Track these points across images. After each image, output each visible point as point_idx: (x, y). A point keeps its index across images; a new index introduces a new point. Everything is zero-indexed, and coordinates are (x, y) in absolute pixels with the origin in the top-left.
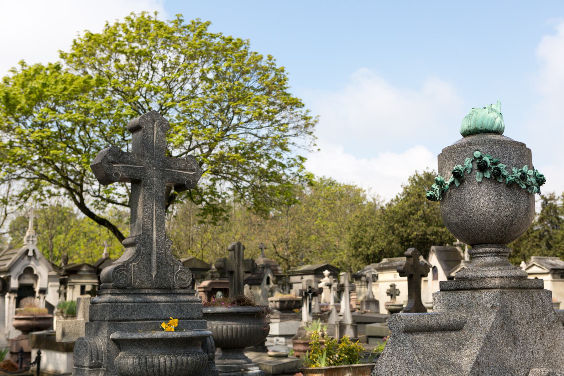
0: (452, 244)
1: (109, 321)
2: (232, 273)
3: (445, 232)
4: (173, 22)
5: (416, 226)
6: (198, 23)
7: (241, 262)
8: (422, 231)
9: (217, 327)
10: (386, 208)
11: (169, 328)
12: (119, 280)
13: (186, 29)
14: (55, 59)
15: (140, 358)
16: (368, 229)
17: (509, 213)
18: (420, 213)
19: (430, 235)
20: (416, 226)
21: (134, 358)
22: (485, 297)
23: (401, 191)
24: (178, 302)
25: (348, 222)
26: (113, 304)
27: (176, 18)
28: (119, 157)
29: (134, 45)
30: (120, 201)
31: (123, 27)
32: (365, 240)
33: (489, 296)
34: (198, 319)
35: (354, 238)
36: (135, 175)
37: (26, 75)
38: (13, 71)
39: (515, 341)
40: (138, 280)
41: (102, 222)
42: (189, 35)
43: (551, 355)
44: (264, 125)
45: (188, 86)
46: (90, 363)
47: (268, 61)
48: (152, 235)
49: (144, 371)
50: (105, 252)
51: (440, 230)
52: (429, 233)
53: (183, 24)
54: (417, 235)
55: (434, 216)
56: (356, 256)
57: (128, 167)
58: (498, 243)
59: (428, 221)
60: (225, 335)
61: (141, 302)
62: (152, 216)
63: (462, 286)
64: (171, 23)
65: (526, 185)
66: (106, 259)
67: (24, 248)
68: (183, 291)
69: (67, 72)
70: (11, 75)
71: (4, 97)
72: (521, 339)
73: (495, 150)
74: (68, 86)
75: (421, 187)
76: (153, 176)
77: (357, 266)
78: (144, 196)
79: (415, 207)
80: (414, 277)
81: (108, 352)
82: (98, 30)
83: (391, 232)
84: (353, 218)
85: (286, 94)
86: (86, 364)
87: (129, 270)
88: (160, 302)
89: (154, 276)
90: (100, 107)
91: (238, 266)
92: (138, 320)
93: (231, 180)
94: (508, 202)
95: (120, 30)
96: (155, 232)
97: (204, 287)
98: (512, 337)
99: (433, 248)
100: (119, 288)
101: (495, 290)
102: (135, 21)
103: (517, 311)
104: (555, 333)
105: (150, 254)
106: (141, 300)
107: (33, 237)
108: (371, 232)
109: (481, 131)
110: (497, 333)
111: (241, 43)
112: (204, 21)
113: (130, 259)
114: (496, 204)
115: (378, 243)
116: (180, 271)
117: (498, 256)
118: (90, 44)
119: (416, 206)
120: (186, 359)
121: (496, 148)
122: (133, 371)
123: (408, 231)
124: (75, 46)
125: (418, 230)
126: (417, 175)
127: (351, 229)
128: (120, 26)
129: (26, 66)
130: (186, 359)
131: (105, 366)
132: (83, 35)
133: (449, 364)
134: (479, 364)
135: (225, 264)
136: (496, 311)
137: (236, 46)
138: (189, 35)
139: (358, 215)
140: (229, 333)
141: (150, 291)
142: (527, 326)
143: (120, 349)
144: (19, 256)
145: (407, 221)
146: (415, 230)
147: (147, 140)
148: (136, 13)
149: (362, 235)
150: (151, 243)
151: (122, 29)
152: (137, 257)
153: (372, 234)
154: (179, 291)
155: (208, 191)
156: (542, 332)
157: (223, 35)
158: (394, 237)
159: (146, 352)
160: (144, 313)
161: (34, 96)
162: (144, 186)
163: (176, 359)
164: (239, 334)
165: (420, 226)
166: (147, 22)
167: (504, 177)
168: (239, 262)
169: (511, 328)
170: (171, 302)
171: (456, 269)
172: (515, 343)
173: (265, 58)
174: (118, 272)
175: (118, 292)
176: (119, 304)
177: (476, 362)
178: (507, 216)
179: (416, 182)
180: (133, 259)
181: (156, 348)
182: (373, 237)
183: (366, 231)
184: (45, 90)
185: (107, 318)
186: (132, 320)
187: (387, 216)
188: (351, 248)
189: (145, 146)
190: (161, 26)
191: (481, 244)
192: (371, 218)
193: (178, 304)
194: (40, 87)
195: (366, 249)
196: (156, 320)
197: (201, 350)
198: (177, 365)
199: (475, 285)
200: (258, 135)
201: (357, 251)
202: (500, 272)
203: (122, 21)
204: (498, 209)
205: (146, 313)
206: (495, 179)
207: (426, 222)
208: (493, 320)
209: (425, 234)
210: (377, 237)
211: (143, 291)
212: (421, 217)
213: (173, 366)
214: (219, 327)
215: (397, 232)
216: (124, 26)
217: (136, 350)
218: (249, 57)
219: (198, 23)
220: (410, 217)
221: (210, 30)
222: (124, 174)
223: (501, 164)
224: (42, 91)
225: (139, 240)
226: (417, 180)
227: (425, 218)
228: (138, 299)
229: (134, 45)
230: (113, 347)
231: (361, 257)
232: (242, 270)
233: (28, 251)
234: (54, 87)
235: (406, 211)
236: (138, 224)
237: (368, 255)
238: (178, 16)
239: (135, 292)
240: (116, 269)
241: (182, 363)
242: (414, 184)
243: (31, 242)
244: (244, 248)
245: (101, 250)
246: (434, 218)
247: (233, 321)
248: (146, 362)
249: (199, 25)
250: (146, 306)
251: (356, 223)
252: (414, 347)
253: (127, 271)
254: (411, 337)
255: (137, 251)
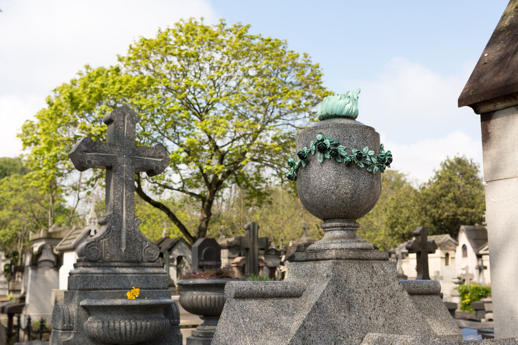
0: (481, 224)
1: (80, 290)
2: (247, 249)
3: (475, 212)
4: (217, 26)
5: (447, 208)
6: (239, 27)
7: (256, 240)
8: (453, 211)
9: (197, 297)
10: (419, 191)
11: (132, 297)
12: (90, 254)
13: (229, 32)
14: (115, 63)
15: (104, 322)
16: (403, 210)
17: (348, 191)
18: (451, 195)
19: (460, 215)
20: (447, 208)
21: (98, 322)
22: (324, 267)
23: (433, 175)
24: (145, 274)
25: (385, 204)
26: (84, 275)
27: (219, 23)
28: (92, 147)
29: (183, 48)
30: (175, 187)
31: (174, 32)
32: (400, 220)
33: (326, 266)
34: (163, 288)
35: (390, 218)
36: (107, 162)
37: (89, 77)
38: (80, 74)
39: (350, 307)
40: (108, 254)
41: (157, 205)
42: (232, 38)
43: (392, 322)
44: (299, 117)
45: (233, 83)
46: (62, 326)
47: (304, 59)
48: (122, 214)
49: (107, 334)
50: (164, 231)
51: (470, 210)
52: (459, 213)
53: (226, 28)
54: (448, 216)
55: (464, 197)
56: (392, 235)
57: (100, 155)
58: (344, 218)
59: (459, 203)
60: (204, 304)
61: (110, 273)
62: (123, 198)
63: (310, 257)
64: (215, 27)
65: (364, 164)
66: (166, 238)
67: (86, 229)
68: (150, 264)
69: (126, 74)
70: (78, 77)
71: (68, 96)
72: (357, 307)
73: (336, 133)
74: (123, 87)
75: (451, 171)
76: (124, 164)
77: (394, 245)
78: (115, 180)
79: (446, 190)
80: (422, 254)
81: (78, 316)
82: (152, 35)
83: (423, 213)
84: (389, 200)
85: (321, 88)
86: (60, 327)
87: (101, 245)
88: (128, 274)
89: (123, 251)
90: (151, 104)
91: (253, 243)
92: (106, 289)
93: (272, 167)
94: (346, 181)
95: (170, 35)
96: (124, 212)
97: (237, 263)
98: (346, 305)
99: (463, 227)
100: (90, 261)
101: (330, 261)
102: (183, 26)
103: (354, 280)
104: (398, 301)
105: (120, 232)
106: (109, 271)
107: (94, 219)
108: (406, 212)
109: (332, 116)
110: (328, 300)
111: (280, 43)
112: (244, 24)
113: (101, 236)
114: (336, 182)
115: (413, 223)
116: (149, 247)
117: (344, 230)
118: (144, 48)
119: (447, 188)
120: (145, 323)
121: (337, 132)
122: (97, 334)
123: (440, 212)
124: (131, 51)
125: (449, 211)
126: (448, 160)
127: (388, 211)
128: (171, 32)
129: (91, 69)
130: (145, 323)
131: (76, 329)
132: (138, 40)
133: (276, 327)
134: (305, 328)
135: (241, 242)
136: (329, 279)
137: (274, 46)
138: (232, 38)
139: (394, 197)
140: (208, 303)
141: (119, 264)
142: (364, 294)
143: (89, 315)
144: (82, 236)
145: (438, 203)
146: (446, 211)
147: (118, 131)
148: (184, 19)
149: (397, 216)
150: (121, 222)
151: (172, 34)
152: (107, 234)
153: (407, 215)
154: (147, 264)
155: (254, 176)
156: (383, 300)
157: (262, 37)
158: (427, 218)
159: (109, 317)
160: (112, 283)
161: (94, 95)
162: (115, 172)
163: (136, 324)
164: (217, 303)
165: (451, 207)
166: (194, 27)
167: (343, 157)
168: (254, 240)
169: (345, 295)
170: (138, 274)
171: (484, 247)
172: (349, 310)
173: (301, 56)
174: (90, 247)
175: (89, 265)
176: (90, 275)
177: (303, 325)
178: (346, 193)
179: (447, 167)
180: (104, 236)
181: (118, 314)
182: (408, 218)
183: (401, 212)
184: (103, 89)
185: (78, 288)
186: (101, 289)
187: (420, 198)
188: (388, 228)
189: (117, 135)
190: (206, 30)
191: (329, 219)
192: (406, 200)
193: (145, 275)
194: (99, 88)
195: (401, 229)
196: (124, 289)
197: (163, 316)
198: (136, 329)
199: (319, 257)
200: (296, 126)
201: (393, 230)
202: (340, 245)
203: (172, 27)
204: (337, 187)
205: (114, 283)
206: (335, 159)
207: (456, 203)
208: (324, 288)
209: (455, 214)
210: (412, 217)
211: (113, 264)
212: (452, 198)
213: (132, 330)
214: (199, 297)
215: (429, 213)
216: (174, 31)
217: (101, 315)
218: (287, 55)
219: (239, 27)
220: (441, 199)
221: (251, 32)
222: (96, 161)
223: (341, 146)
224: (101, 91)
225: (110, 219)
226: (448, 164)
227: (455, 199)
228: (107, 271)
229: (183, 48)
230: (83, 313)
231: (397, 236)
232: (257, 247)
233: (90, 231)
234: (111, 87)
235: (438, 194)
236: (110, 205)
237: (403, 235)
238: (221, 20)
239: (105, 264)
240: (87, 244)
241: (142, 327)
242: (446, 168)
243: (93, 224)
244: (259, 227)
245: (161, 230)
246: (465, 200)
247: (211, 292)
248: (108, 326)
249: (241, 28)
250: (114, 277)
251: (392, 205)
252: (242, 312)
253: (98, 247)
254: (242, 302)
255: (108, 229)
